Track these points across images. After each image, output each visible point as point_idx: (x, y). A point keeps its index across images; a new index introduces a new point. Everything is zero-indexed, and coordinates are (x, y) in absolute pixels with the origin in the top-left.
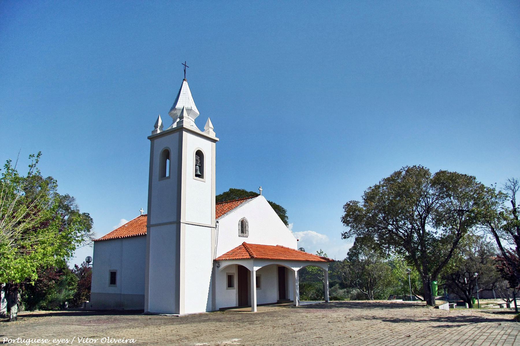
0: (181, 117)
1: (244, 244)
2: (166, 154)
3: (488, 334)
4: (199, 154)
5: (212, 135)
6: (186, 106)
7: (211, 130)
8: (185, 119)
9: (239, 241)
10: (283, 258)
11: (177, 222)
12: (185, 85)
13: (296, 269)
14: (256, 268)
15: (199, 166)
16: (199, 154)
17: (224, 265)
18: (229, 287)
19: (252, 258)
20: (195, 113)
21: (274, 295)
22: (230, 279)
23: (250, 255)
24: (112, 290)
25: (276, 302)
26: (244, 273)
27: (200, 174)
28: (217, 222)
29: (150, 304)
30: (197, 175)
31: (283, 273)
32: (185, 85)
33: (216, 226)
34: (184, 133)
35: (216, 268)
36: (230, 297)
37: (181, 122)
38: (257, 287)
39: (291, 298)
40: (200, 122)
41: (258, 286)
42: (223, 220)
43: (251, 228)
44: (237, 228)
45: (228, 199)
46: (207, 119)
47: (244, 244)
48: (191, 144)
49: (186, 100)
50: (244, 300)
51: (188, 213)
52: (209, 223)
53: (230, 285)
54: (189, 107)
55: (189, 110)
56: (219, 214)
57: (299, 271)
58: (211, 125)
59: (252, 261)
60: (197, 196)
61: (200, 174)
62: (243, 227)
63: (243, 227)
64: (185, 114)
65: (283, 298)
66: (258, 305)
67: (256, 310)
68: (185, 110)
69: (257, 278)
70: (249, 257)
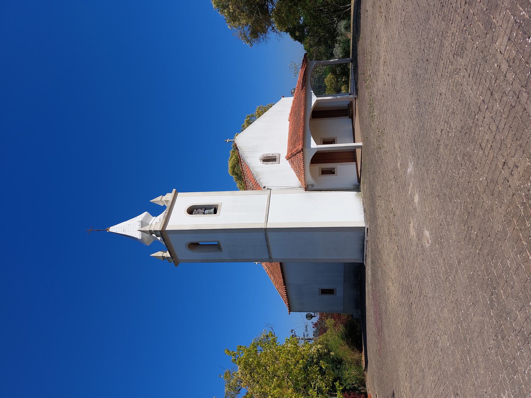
0: (151, 232)
1: (288, 158)
2: (194, 246)
3: (486, 152)
4: (191, 211)
5: (169, 197)
6: (139, 228)
7: (164, 198)
8: (152, 229)
9: (285, 164)
10: (302, 114)
11: (265, 233)
12: (114, 229)
13: (314, 99)
14: (313, 145)
15: (205, 209)
16: (191, 211)
17: (310, 180)
18: (334, 173)
19: (302, 150)
20: (146, 217)
21: (343, 123)
22: (325, 172)
23: (300, 152)
24: (340, 291)
25: (351, 119)
26: (319, 158)
27: (215, 210)
28: (264, 187)
29: (352, 257)
30: (215, 212)
31: (320, 113)
32: (114, 229)
33: (268, 189)
34: (168, 228)
35: (314, 188)
36: (347, 171)
37: (155, 232)
38: (332, 143)
39: (346, 104)
40: (156, 210)
41: (332, 142)
42: (264, 181)
43: (270, 152)
44: (270, 166)
45: (240, 178)
46: (153, 204)
47: (288, 158)
48: (180, 220)
49: (130, 228)
50: (349, 156)
51: (256, 221)
52: (266, 197)
53: (331, 172)
54: (139, 223)
55: (143, 224)
56: (257, 186)
57: (317, 95)
58: (159, 199)
59: (306, 150)
60: (235, 211)
61: (215, 210)
62: (269, 159)
63: (269, 159)
64: (147, 228)
65: (346, 112)
66: (354, 142)
67: (360, 144)
68: (142, 229)
69: (325, 143)
70: (300, 155)
